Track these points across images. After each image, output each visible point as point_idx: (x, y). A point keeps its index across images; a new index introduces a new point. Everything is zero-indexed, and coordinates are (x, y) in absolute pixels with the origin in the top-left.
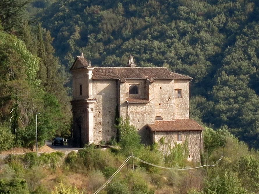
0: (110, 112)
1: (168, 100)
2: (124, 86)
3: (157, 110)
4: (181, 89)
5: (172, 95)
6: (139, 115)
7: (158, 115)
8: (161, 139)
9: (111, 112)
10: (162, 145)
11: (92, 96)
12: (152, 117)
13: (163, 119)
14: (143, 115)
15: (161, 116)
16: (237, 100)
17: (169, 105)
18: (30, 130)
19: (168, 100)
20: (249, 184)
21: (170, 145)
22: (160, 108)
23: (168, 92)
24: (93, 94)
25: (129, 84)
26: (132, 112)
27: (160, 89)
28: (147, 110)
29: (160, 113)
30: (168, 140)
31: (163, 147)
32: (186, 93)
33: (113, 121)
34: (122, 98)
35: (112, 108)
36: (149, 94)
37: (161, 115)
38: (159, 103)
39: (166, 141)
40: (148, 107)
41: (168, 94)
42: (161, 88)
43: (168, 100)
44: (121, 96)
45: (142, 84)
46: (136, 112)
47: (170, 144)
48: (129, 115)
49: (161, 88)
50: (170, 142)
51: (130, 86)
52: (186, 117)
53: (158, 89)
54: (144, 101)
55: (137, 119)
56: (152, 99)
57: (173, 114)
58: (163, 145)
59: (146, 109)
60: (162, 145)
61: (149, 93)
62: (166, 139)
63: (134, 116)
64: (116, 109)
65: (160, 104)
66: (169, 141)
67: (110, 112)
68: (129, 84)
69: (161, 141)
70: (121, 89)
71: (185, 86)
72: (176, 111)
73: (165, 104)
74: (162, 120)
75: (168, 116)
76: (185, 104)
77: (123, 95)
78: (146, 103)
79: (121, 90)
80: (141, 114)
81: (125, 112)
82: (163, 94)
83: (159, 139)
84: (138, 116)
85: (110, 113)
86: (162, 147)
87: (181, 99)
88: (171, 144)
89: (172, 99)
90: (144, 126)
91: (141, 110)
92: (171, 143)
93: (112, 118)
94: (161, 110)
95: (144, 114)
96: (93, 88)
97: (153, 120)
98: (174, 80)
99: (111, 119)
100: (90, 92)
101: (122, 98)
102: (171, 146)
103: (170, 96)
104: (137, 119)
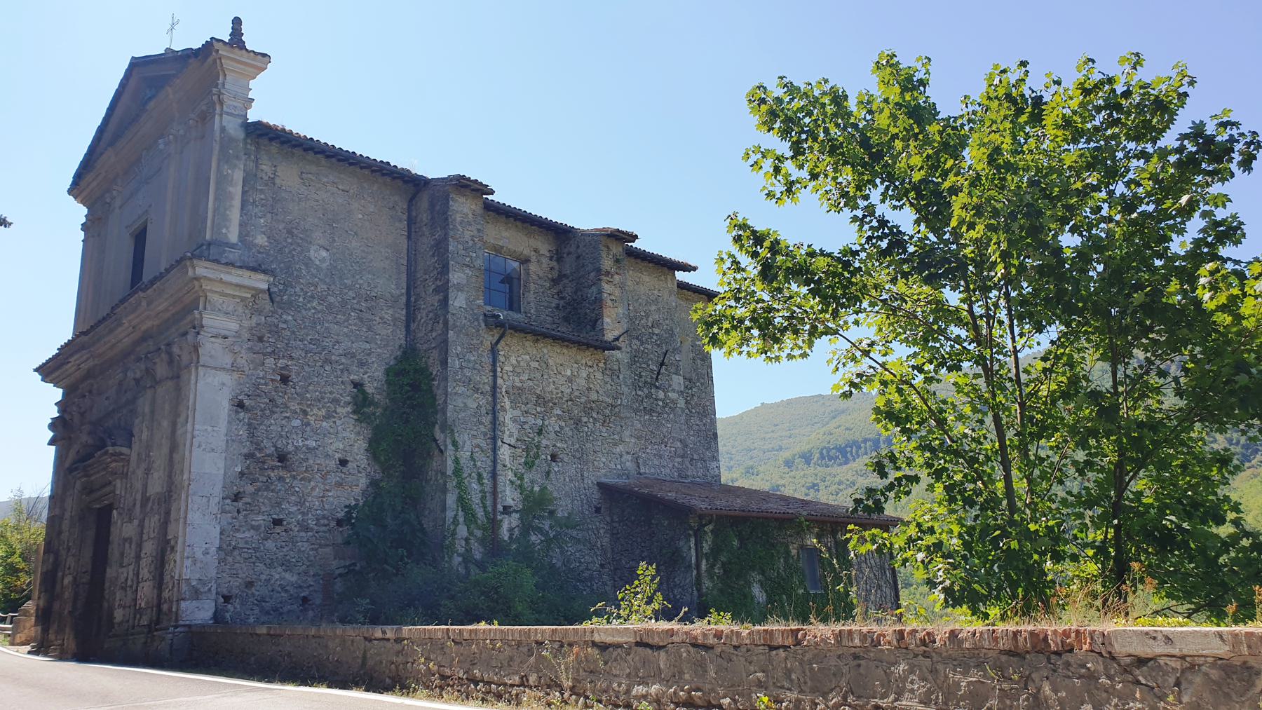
11: (233, 246)
26: (517, 394)
46: (540, 400)
56: (616, 333)
77: (467, 271)
96: (244, 193)
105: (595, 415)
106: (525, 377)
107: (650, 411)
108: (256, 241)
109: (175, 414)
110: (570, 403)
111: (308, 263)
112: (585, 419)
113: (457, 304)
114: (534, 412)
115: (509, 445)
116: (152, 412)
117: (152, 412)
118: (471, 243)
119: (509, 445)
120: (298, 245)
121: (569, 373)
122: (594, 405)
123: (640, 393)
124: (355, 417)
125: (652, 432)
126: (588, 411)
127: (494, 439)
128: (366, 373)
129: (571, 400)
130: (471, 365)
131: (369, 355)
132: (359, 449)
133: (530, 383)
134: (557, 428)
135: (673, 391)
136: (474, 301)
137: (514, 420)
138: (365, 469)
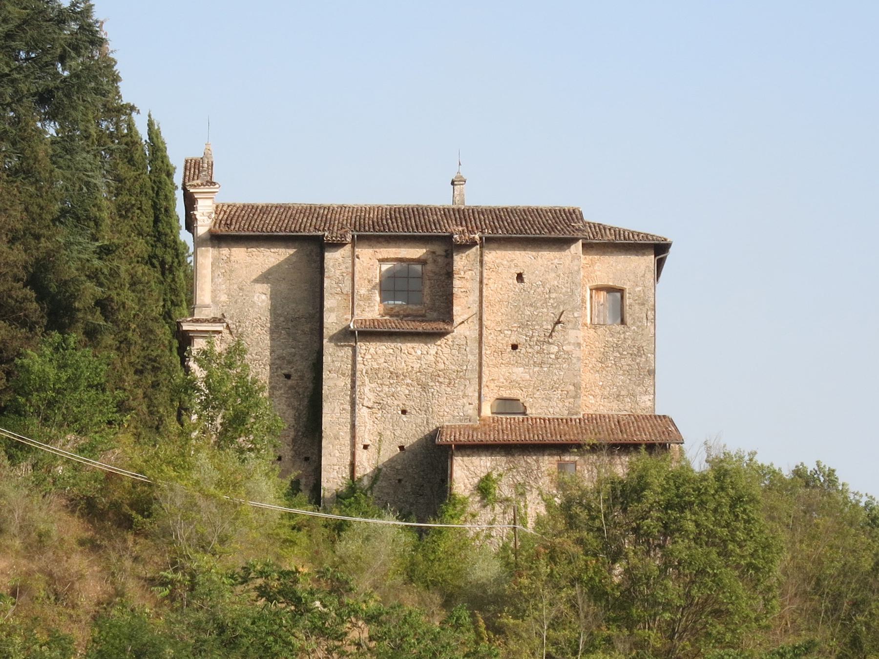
0: (288, 376)
1: (550, 327)
2: (340, 260)
3: (504, 369)
4: (618, 284)
5: (568, 307)
6: (407, 385)
7: (506, 394)
8: (482, 480)
9: (295, 376)
10: (489, 507)
11: (207, 306)
12: (464, 396)
13: (528, 412)
14: (424, 387)
15: (520, 397)
16: (44, 125)
17: (554, 349)
18: (151, 523)
19: (553, 330)
20: (642, 597)
21: (525, 506)
22: (517, 364)
23: (553, 295)
24: (214, 301)
25: (382, 261)
26: (374, 374)
27: (515, 282)
28: (442, 366)
29: (512, 383)
30: (516, 486)
31: (490, 517)
32: (643, 304)
33: (299, 417)
34: (332, 310)
35: (297, 358)
36: (452, 294)
37: (519, 392)
38: (513, 340)
39: (504, 490)
40: (446, 350)
41: (552, 301)
42: (520, 277)
43: (553, 330)
44: (328, 303)
45: (435, 261)
46: (394, 375)
47: (522, 504)
48: (363, 384)
49: (520, 277)
50: (522, 494)
51: (385, 267)
52: (643, 405)
53: (510, 281)
54: (441, 326)
55: (396, 402)
56: (465, 317)
57: (572, 388)
58: (493, 509)
59: (437, 362)
60: (485, 506)
61: (455, 290)
62: (504, 480)
63: (386, 389)
64: (314, 364)
65: (514, 347)
66: (521, 490)
67: (288, 376)
68: (382, 261)
69: (484, 489)
70: (326, 274)
71: (636, 276)
72: (587, 377)
73: (537, 348)
74: (524, 413)
75: (550, 399)
76: (639, 351)
77: (337, 297)
78: (441, 334)
79: (329, 277)
80: (418, 380)
81: (343, 375)
82: (531, 305)
83: (476, 480)
84: (403, 390)
85: (290, 382)
86: (486, 515)
87: (620, 328)
88: (530, 505)
89: (570, 326)
90: (427, 432)
91: (417, 366)
92: (529, 498)
93: (296, 404)
94: (521, 369)
95: (431, 384)
96: (213, 271)
97: (467, 406)
98: (580, 242)
99: (293, 408)
100: (202, 290)
101: (332, 310)
102: (526, 514)
103: (562, 313)
104: (396, 402)
105: (440, 380)
106: (382, 360)
107: (541, 364)
108: (221, 299)
109: (451, 480)
110: (419, 374)
111: (254, 304)
112: (431, 384)
113: (330, 321)
114: (388, 383)
115: (367, 407)
116: (626, 448)
117: (626, 448)
118: (341, 278)
119: (367, 407)
120: (246, 296)
121: (419, 352)
122: (440, 373)
123: (530, 350)
124: (286, 396)
125: (541, 381)
126: (434, 377)
127: (353, 404)
128: (293, 367)
129: (420, 372)
130: (339, 359)
131: (294, 356)
132: (289, 415)
133: (386, 364)
134: (407, 392)
135: (569, 343)
136: (343, 316)
137: (372, 390)
138: (293, 426)
